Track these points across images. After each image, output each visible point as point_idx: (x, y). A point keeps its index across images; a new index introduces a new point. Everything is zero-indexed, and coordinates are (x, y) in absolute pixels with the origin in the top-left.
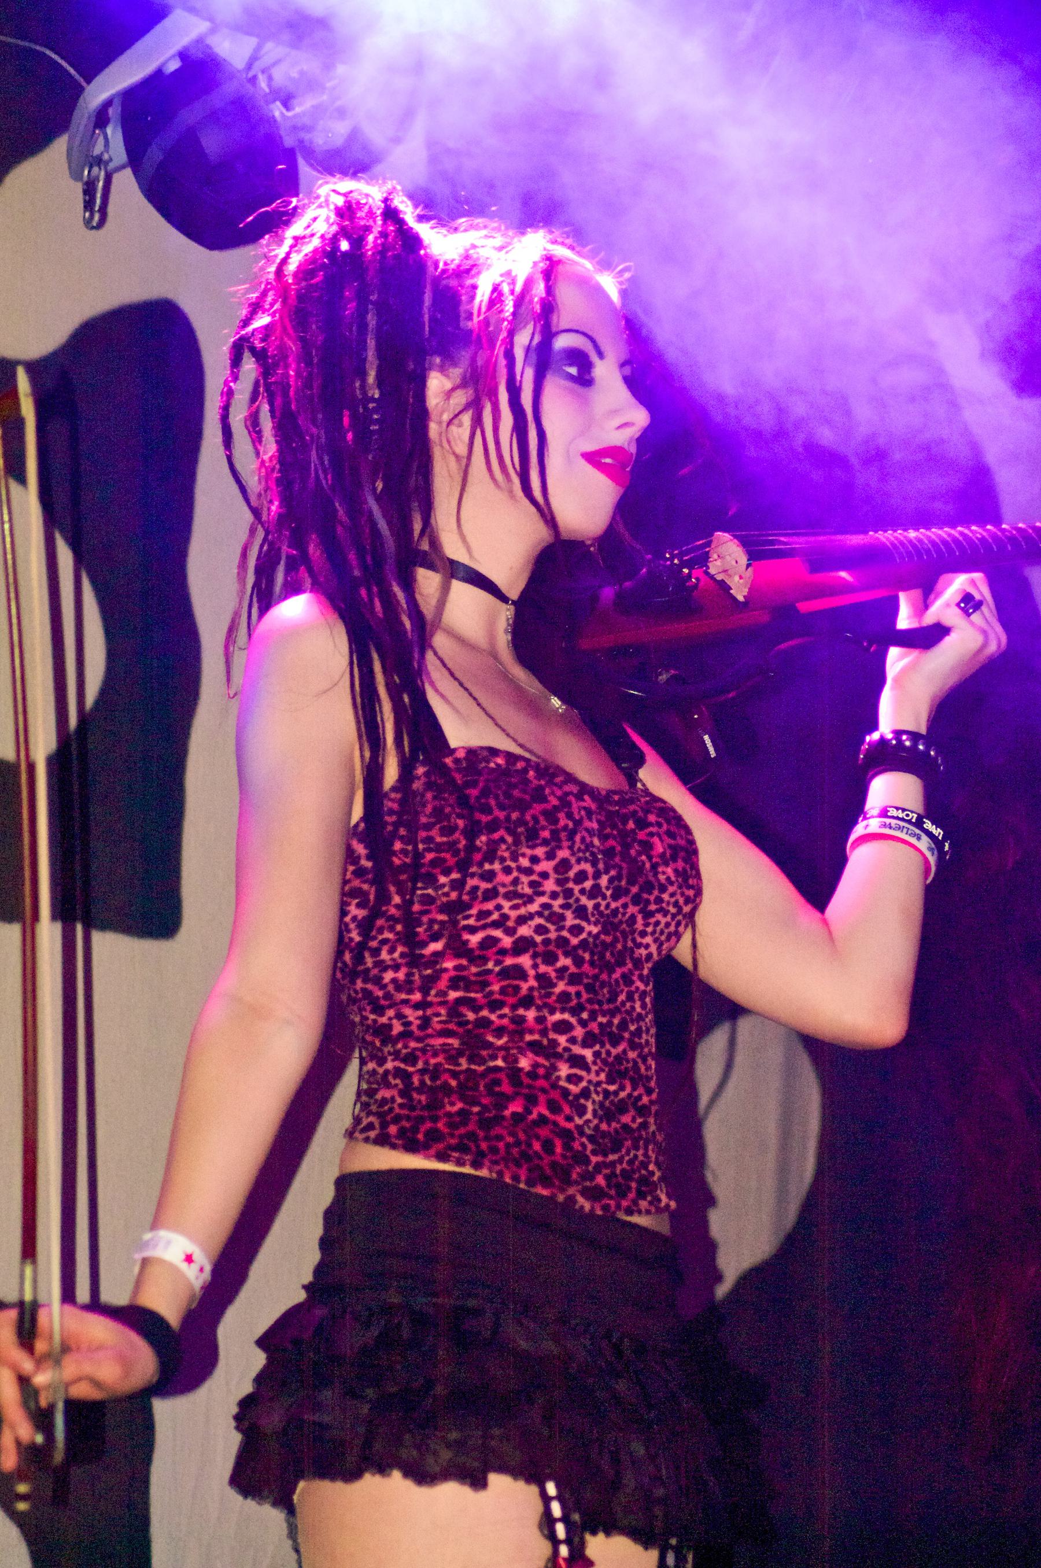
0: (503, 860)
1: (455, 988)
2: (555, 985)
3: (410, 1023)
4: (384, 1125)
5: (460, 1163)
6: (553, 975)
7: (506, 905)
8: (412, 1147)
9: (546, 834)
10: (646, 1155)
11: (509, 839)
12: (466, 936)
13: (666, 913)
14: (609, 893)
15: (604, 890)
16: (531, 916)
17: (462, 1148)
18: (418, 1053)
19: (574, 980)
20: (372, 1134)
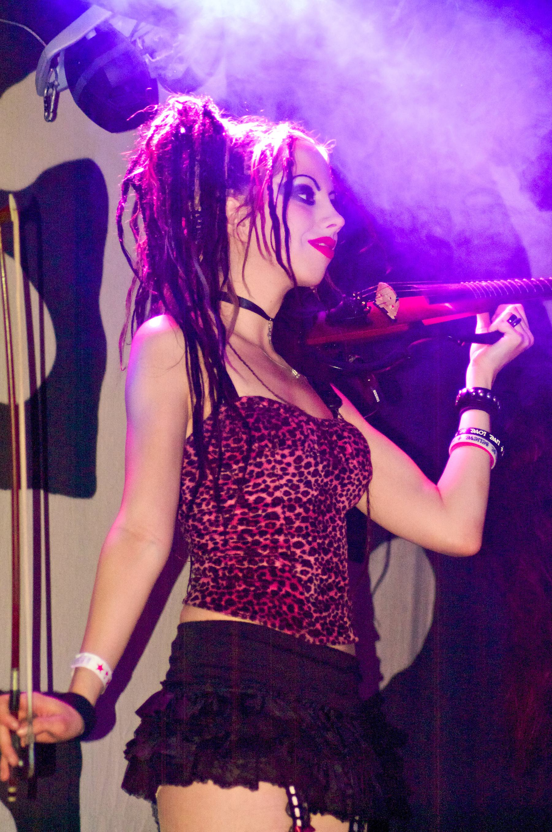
0: (267, 456)
1: (241, 524)
2: (294, 523)
3: (217, 543)
4: (204, 597)
5: (244, 617)
6: (293, 517)
7: (268, 480)
8: (218, 609)
9: (289, 443)
10: (342, 613)
11: (270, 445)
12: (247, 497)
13: (353, 484)
14: (323, 474)
15: (320, 472)
16: (282, 486)
17: (245, 609)
18: (222, 559)
19: (304, 520)
20: (197, 602)
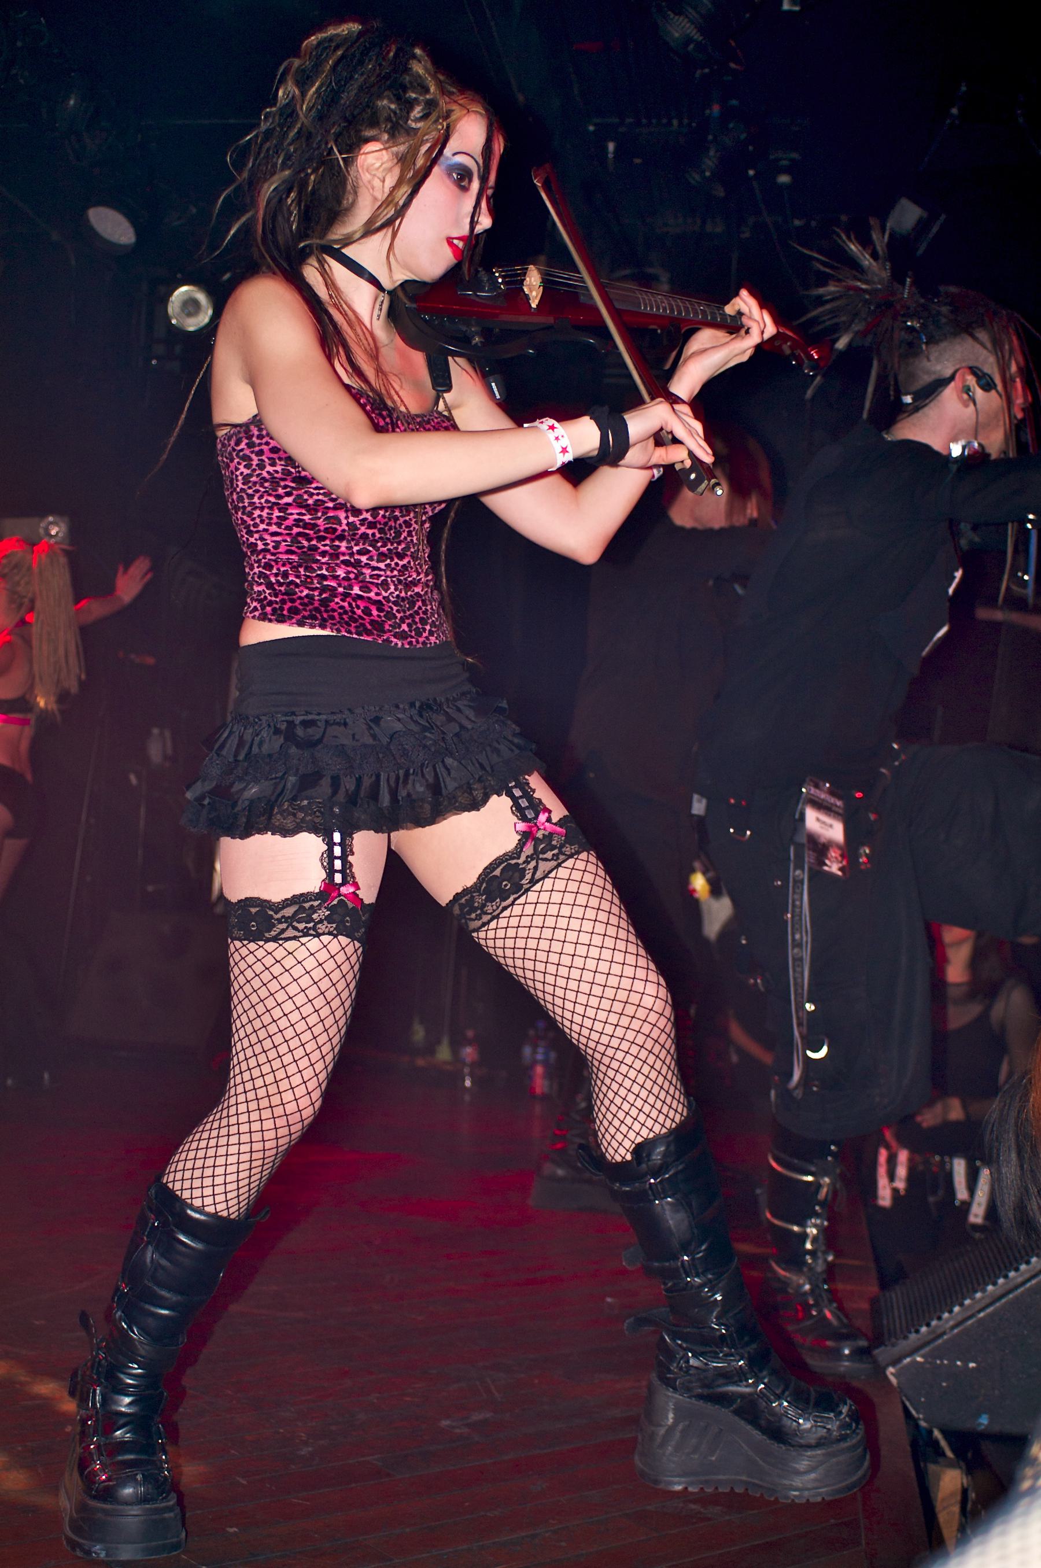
1: (298, 526)
3: (268, 544)
4: (263, 608)
5: (312, 627)
10: (432, 608)
18: (273, 563)
20: (257, 614)
